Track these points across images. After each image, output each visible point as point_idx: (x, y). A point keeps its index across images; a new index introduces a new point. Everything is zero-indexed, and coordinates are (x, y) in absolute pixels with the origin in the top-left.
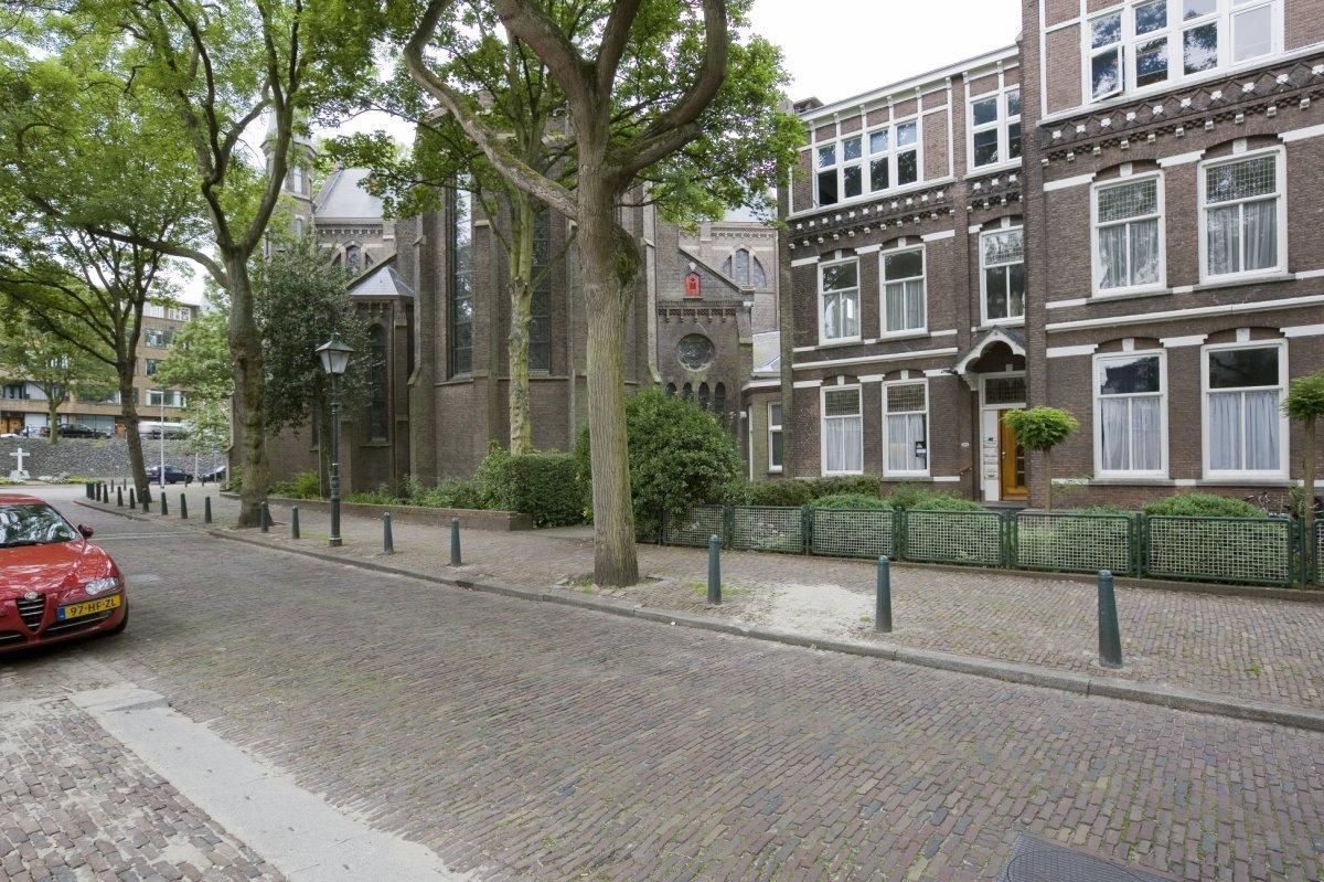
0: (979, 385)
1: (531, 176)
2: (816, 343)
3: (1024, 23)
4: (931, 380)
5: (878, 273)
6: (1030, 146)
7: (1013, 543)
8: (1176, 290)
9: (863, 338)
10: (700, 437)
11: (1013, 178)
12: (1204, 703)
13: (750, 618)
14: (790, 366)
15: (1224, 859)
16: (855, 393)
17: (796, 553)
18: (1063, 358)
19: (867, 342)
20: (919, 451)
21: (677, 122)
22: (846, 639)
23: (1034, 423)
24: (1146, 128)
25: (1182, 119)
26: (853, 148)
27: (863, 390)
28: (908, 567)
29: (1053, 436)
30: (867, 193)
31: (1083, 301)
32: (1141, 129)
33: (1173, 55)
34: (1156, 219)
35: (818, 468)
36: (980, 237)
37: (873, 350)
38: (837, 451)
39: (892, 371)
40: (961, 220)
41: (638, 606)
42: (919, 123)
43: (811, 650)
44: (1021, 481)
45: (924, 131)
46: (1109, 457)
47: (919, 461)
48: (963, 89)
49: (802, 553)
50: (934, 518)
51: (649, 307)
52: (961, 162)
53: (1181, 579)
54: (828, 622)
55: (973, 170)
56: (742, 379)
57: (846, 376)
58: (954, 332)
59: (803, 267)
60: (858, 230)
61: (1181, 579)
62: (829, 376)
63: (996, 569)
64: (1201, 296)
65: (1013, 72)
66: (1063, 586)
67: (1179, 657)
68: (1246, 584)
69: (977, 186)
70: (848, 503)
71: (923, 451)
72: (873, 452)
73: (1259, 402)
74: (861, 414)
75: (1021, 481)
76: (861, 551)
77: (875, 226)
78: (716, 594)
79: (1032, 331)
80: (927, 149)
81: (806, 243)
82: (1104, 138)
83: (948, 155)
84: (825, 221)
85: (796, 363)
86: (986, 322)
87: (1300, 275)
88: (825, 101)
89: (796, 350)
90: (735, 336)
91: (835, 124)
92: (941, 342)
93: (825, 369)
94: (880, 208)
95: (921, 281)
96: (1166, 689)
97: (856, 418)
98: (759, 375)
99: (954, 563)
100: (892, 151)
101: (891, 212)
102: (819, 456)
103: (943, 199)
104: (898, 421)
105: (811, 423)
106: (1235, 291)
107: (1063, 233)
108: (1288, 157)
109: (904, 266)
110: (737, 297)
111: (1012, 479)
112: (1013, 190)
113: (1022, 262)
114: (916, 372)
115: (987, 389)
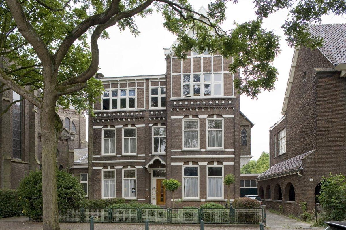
0: (151, 171)
1: (17, 86)
2: (101, 155)
4: (138, 169)
6: (168, 105)
7: (170, 217)
9: (116, 154)
10: (72, 185)
11: (162, 112)
14: (91, 161)
16: (134, 172)
19: (118, 156)
20: (133, 191)
21: (80, 81)
23: (170, 183)
24: (196, 107)
25: (204, 107)
26: (115, 93)
27: (116, 171)
28: (142, 225)
29: (175, 187)
30: (119, 109)
31: (180, 150)
34: (197, 131)
35: (100, 196)
38: (107, 191)
40: (147, 122)
42: (136, 90)
44: (162, 200)
45: (137, 93)
46: (186, 193)
47: (133, 194)
49: (109, 222)
50: (148, 210)
51: (35, 135)
52: (147, 105)
53: (209, 224)
55: (151, 108)
56: (70, 164)
57: (110, 166)
58: (144, 155)
60: (116, 120)
62: (105, 166)
64: (207, 152)
65: (162, 82)
66: (184, 227)
68: (222, 224)
69: (152, 113)
71: (135, 191)
72: (119, 191)
73: (218, 180)
74: (115, 179)
75: (162, 200)
76: (127, 221)
77: (121, 119)
79: (167, 157)
81: (103, 121)
83: (144, 102)
84: (105, 115)
86: (154, 153)
87: (227, 150)
89: (94, 156)
90: (67, 149)
92: (141, 158)
93: (103, 163)
94: (123, 114)
95: (135, 138)
97: (114, 180)
98: (76, 163)
99: (154, 223)
102: (101, 192)
103: (142, 115)
104: (127, 181)
107: (176, 131)
110: (68, 135)
111: (160, 200)
112: (162, 116)
113: (165, 137)
114: (133, 166)
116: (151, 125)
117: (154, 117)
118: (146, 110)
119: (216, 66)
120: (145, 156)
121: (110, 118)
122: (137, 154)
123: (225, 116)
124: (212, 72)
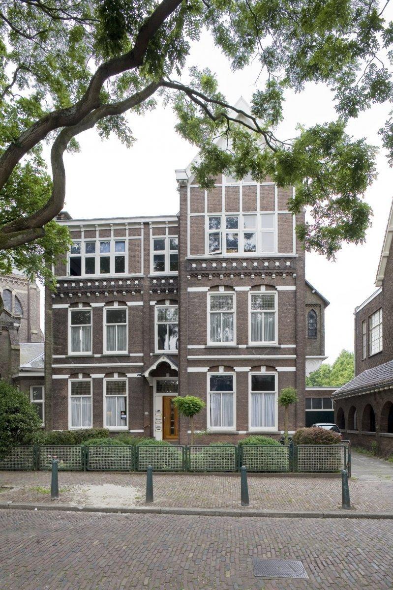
0: (153, 383)
2: (66, 353)
3: (181, 208)
4: (130, 379)
5: (103, 318)
7: (188, 461)
8: (240, 346)
9: (93, 353)
12: (279, 514)
13: (79, 502)
14: (50, 365)
15: (309, 552)
16: (88, 383)
17: (77, 471)
18: (195, 372)
19: (96, 356)
20: (123, 416)
22: (133, 507)
26: (91, 247)
28: (140, 474)
30: (98, 274)
31: (203, 347)
32: (228, 272)
33: (242, 242)
34: (232, 313)
35: (66, 425)
36: (155, 308)
37: (99, 360)
38: (77, 417)
39: (109, 374)
40: (146, 297)
41: (10, 502)
43: (118, 514)
46: (213, 421)
47: (122, 422)
48: (149, 231)
49: (83, 470)
50: (150, 449)
52: (147, 268)
53: (254, 472)
54: (121, 501)
55: (153, 273)
56: (12, 371)
58: (142, 355)
59: (59, 309)
60: (93, 293)
61: (254, 472)
62: (74, 373)
63: (180, 473)
67: (265, 499)
68: (276, 472)
70: (105, 443)
72: (98, 416)
74: (91, 395)
76: (114, 468)
77: (102, 293)
78: (55, 491)
80: (130, 257)
82: (214, 272)
84: (74, 285)
85: (54, 364)
86: (157, 351)
87: (282, 346)
88: (74, 216)
89: (54, 356)
91: (81, 231)
92: (135, 360)
93: (71, 369)
94: (105, 283)
95: (125, 326)
96: (266, 511)
98: (23, 369)
100: (112, 254)
101: (111, 286)
102: (67, 418)
103: (138, 285)
104: (112, 400)
105: (62, 399)
106: (261, 350)
108: (279, 297)
109: (115, 316)
111: (168, 431)
112: (172, 287)
114: (122, 374)
115: (157, 385)
116: (152, 303)
117: (159, 288)
118: (144, 276)
119: (264, 202)
120: (143, 357)
121: (82, 291)
122: (130, 352)
123: (279, 288)
124: (258, 212)
